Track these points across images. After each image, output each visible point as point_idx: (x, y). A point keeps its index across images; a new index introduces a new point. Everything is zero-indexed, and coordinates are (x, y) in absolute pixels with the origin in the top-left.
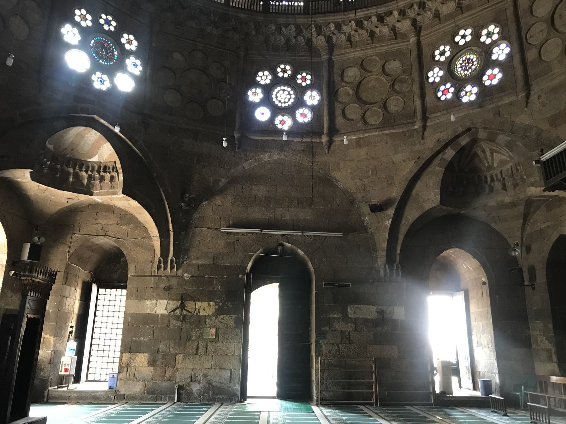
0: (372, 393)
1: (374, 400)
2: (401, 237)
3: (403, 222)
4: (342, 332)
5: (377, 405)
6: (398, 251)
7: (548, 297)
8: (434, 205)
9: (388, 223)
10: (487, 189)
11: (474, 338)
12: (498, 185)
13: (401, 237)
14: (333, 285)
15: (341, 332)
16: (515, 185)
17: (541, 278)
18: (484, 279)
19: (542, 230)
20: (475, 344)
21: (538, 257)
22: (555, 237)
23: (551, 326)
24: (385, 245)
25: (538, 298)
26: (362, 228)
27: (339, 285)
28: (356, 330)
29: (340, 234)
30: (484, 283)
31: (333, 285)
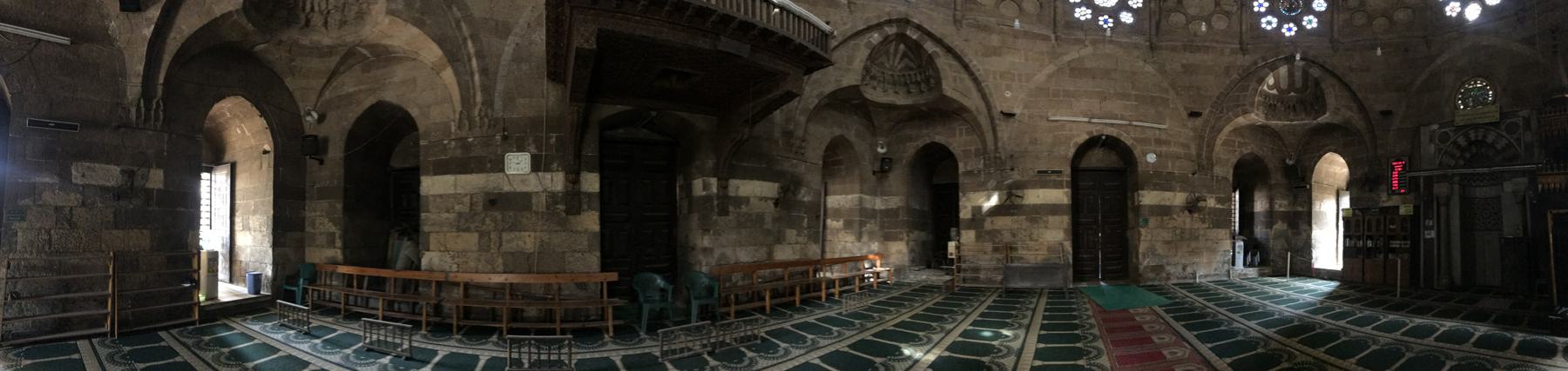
0: (106, 315)
1: (107, 328)
2: (167, 59)
3: (172, 35)
4: (57, 209)
5: (112, 334)
6: (161, 81)
7: (342, 171)
8: (231, 8)
9: (148, 32)
10: (303, 22)
11: (238, 220)
12: (317, 20)
13: (167, 59)
14: (46, 125)
15: (56, 208)
16: (343, 23)
17: (336, 152)
18: (267, 147)
19: (349, 95)
20: (238, 227)
21: (336, 130)
22: (370, 101)
23: (339, 206)
24: (140, 68)
25: (329, 171)
26: (106, 38)
27: (57, 126)
28: (83, 204)
29: (65, 40)
30: (265, 152)
31: (46, 125)
